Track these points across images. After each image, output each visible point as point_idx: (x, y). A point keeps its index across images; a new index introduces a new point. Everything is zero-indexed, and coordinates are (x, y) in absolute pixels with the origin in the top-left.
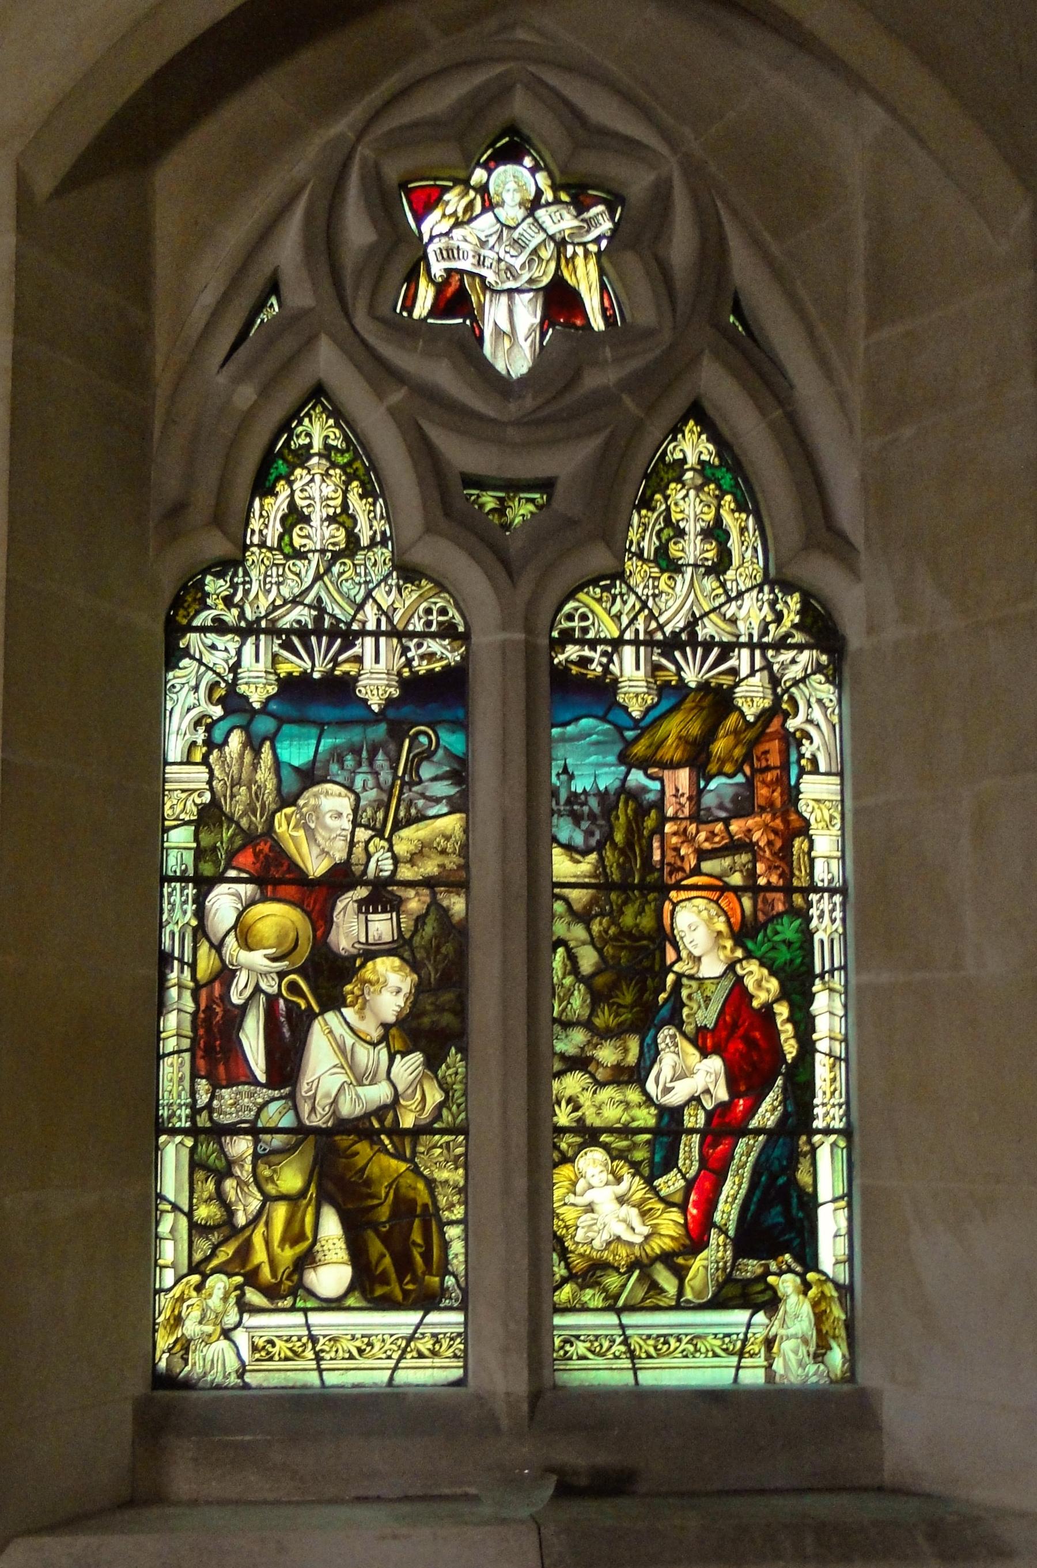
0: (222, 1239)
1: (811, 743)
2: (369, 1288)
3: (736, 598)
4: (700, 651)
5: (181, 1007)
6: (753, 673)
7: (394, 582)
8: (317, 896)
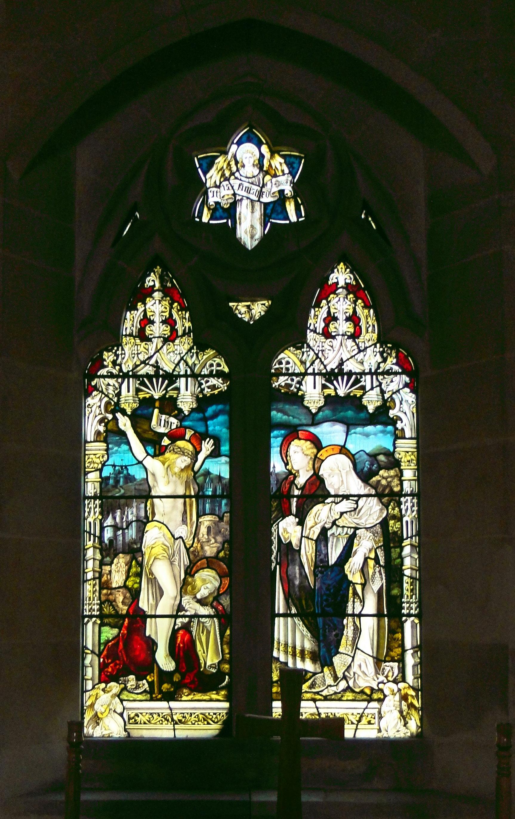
1: (402, 422)
3: (363, 351)
4: (345, 377)
5: (95, 557)
6: (372, 388)
7: (195, 351)
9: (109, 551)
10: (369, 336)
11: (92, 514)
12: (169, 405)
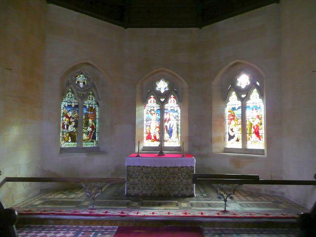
0: (64, 139)
2: (72, 141)
8: (69, 118)
9: (147, 126)
10: (175, 102)
11: (145, 122)
12: (153, 110)
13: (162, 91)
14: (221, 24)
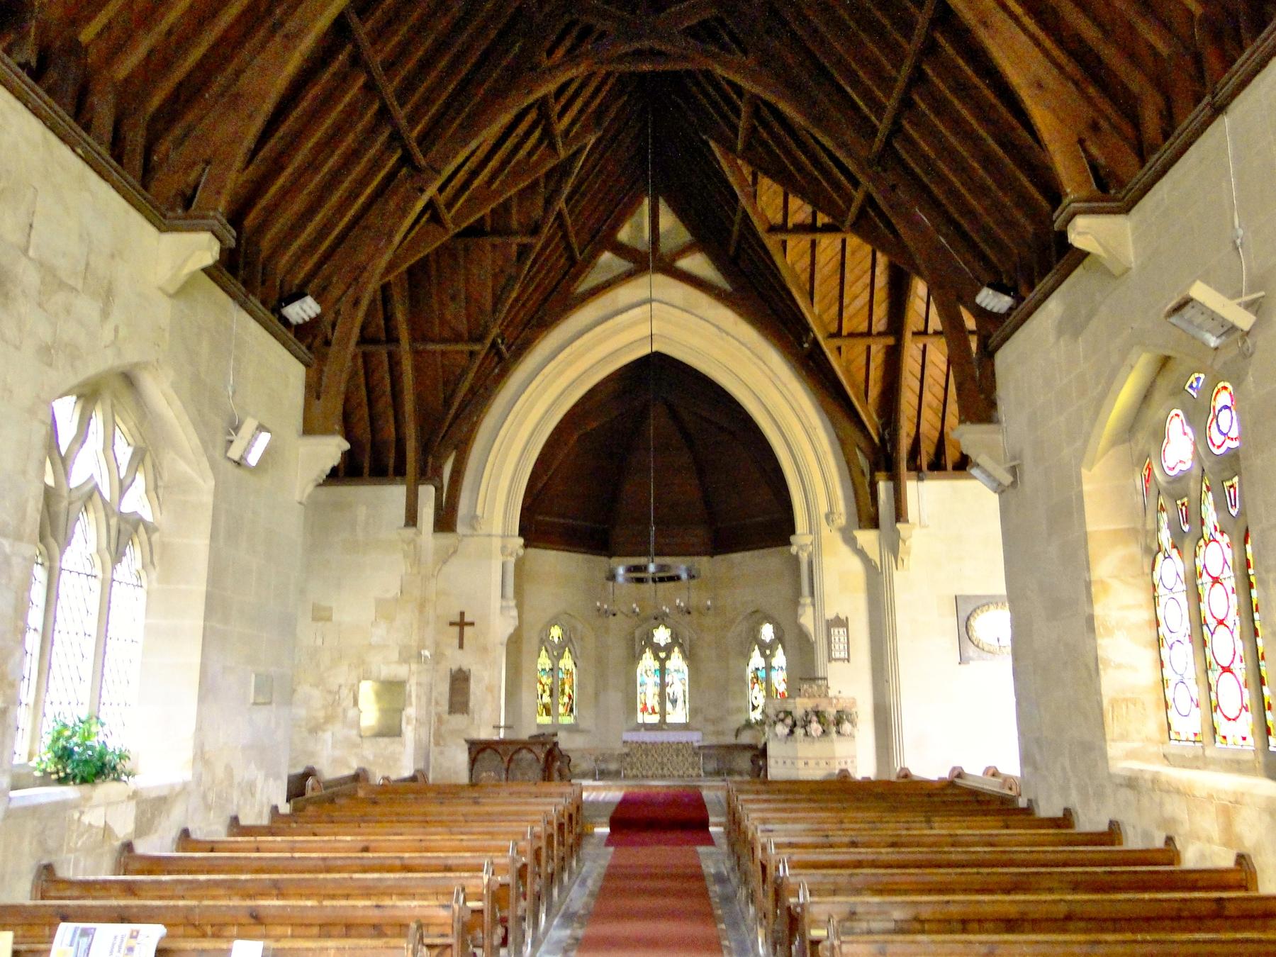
13: (662, 644)
14: (737, 557)
